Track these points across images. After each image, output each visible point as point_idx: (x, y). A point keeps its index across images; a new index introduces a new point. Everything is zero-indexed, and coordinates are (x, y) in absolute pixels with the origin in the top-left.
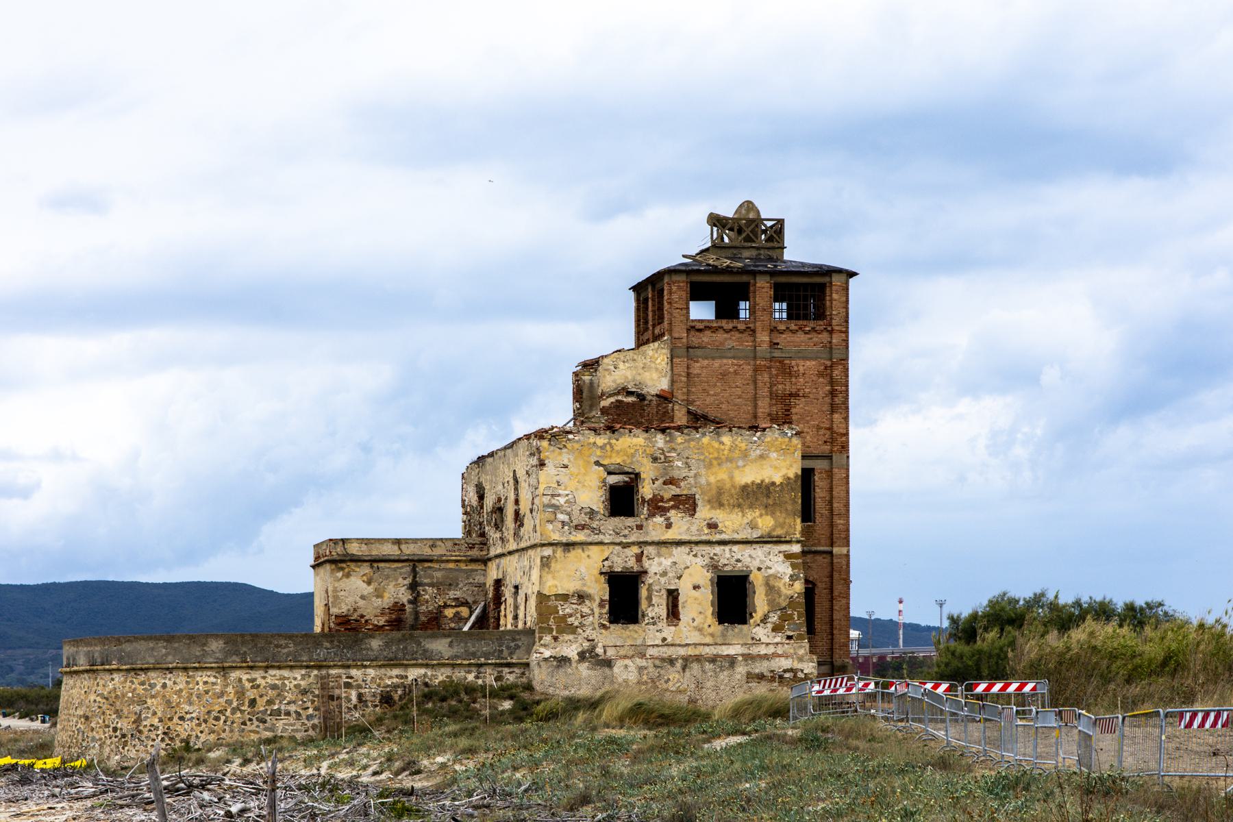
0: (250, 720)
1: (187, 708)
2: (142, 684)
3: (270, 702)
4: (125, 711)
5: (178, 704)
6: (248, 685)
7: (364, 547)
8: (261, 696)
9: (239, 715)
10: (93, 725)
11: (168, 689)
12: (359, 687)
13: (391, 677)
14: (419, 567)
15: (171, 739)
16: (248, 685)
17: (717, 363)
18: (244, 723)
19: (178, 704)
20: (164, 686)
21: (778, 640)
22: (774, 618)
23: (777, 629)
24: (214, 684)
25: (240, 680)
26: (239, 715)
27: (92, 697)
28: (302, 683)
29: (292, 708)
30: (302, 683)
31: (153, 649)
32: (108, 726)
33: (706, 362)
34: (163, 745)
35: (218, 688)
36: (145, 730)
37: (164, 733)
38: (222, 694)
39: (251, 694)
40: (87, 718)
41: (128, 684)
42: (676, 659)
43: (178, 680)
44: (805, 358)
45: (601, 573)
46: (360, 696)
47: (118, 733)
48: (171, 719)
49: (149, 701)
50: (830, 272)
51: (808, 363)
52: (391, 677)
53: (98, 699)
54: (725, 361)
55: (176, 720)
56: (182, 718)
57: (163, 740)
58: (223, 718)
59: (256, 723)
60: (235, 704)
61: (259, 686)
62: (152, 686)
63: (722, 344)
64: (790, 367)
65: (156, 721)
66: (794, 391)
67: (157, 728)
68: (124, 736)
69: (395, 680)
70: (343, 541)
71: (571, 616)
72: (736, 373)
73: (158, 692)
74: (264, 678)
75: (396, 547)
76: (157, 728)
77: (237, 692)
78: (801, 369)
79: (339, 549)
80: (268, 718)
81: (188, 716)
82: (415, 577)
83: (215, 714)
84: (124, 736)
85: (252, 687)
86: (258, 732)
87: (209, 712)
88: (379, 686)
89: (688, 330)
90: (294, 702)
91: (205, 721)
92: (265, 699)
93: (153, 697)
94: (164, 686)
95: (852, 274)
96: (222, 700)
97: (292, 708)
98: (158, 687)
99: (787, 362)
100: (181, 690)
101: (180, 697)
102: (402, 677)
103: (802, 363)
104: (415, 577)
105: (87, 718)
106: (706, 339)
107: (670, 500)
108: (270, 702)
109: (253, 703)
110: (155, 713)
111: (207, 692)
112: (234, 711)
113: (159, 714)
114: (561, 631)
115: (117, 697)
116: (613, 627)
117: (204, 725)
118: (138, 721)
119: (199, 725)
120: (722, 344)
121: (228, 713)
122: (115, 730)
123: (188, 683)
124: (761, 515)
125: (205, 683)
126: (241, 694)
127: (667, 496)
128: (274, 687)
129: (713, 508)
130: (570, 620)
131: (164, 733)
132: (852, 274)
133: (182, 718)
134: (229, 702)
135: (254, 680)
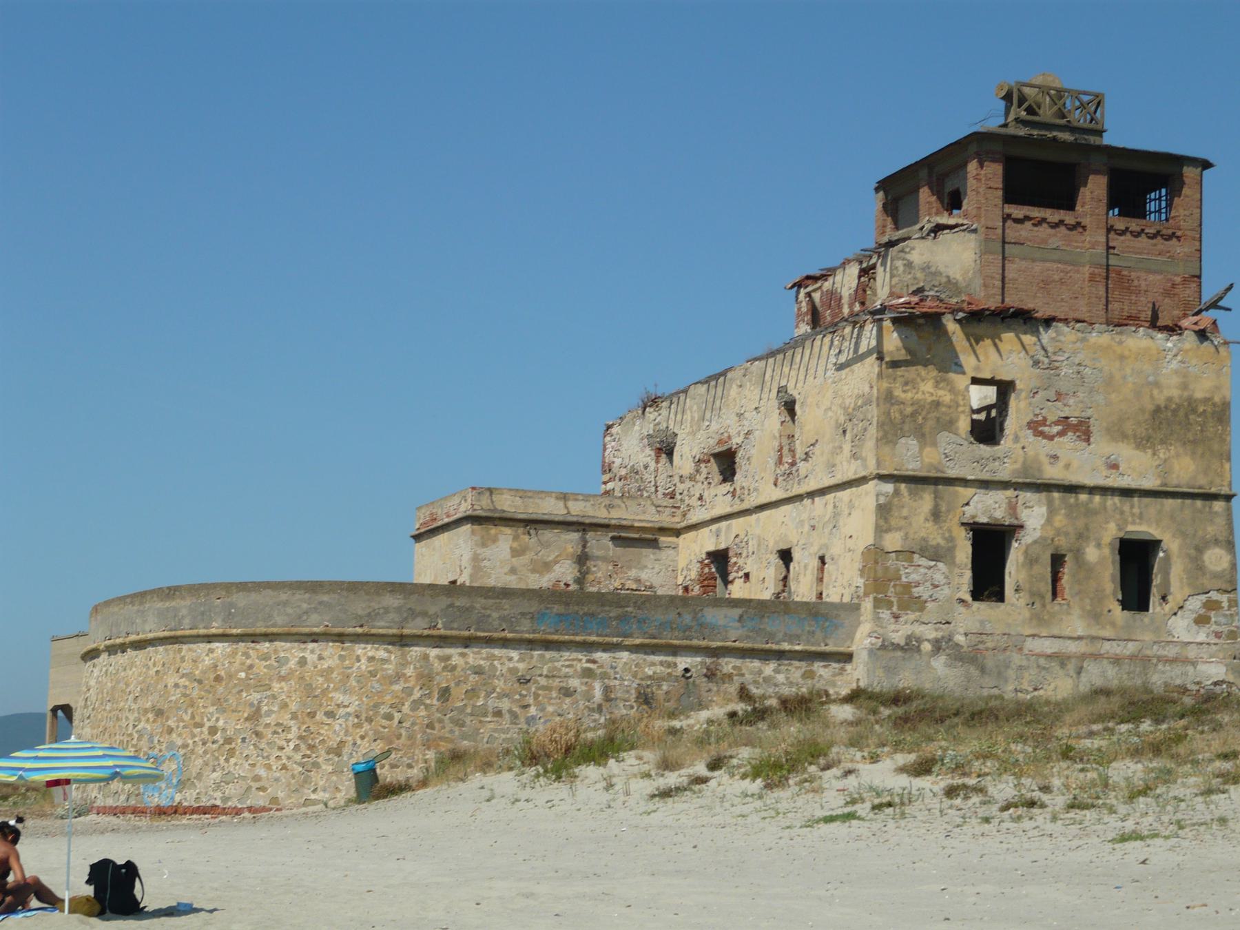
0: (440, 721)
1: (339, 697)
2: (265, 657)
3: (472, 693)
4: (232, 700)
5: (325, 692)
6: (438, 666)
7: (518, 501)
8: (458, 684)
9: (422, 712)
10: (171, 723)
11: (309, 667)
12: (604, 676)
13: (653, 664)
14: (590, 535)
15: (311, 747)
16: (438, 666)
17: (1038, 267)
18: (430, 726)
19: (325, 692)
20: (303, 662)
21: (1201, 637)
22: (1196, 604)
23: (1201, 621)
24: (384, 661)
25: (426, 657)
26: (422, 712)
27: (171, 680)
28: (521, 666)
29: (505, 705)
30: (521, 666)
31: (285, 604)
32: (201, 725)
33: (1024, 264)
34: (298, 757)
35: (390, 668)
36: (268, 733)
37: (301, 738)
38: (398, 676)
39: (443, 680)
40: (159, 713)
41: (239, 657)
42: (1069, 658)
43: (326, 654)
44: (1149, 271)
45: (963, 524)
46: (607, 690)
47: (218, 736)
48: (312, 715)
49: (276, 686)
50: (1180, 161)
51: (1151, 277)
52: (653, 664)
53: (183, 681)
54: (1048, 265)
55: (320, 716)
56: (330, 714)
57: (297, 748)
58: (397, 716)
59: (449, 726)
60: (417, 694)
61: (454, 668)
62: (281, 662)
63: (1044, 241)
64: (1130, 280)
65: (286, 718)
66: (1134, 312)
67: (286, 729)
68: (228, 741)
69: (659, 669)
70: (491, 491)
71: (918, 584)
72: (1062, 282)
73: (292, 672)
74: (463, 655)
75: (561, 504)
76: (286, 729)
77: (420, 676)
78: (1143, 284)
79: (485, 502)
80: (468, 720)
81: (342, 711)
82: (584, 546)
83: (384, 710)
84: (228, 741)
85: (445, 668)
86: (451, 741)
87: (376, 706)
88: (635, 676)
89: (1004, 221)
90: (506, 695)
91: (369, 720)
92: (465, 687)
93: (282, 679)
94: (303, 662)
95: (1206, 165)
96: (397, 687)
97: (505, 705)
98: (292, 664)
99: (1125, 273)
100: (330, 670)
101: (328, 680)
102: (669, 665)
103: (1143, 275)
104: (584, 546)
105: (159, 713)
106: (1024, 233)
107: (1056, 423)
108: (472, 693)
109: (445, 693)
110: (284, 706)
111: (373, 674)
112: (416, 705)
113: (293, 707)
114: (904, 606)
115: (218, 679)
116: (976, 604)
117: (366, 726)
118: (255, 716)
119: (359, 725)
120: (1044, 241)
121: (406, 708)
122: (213, 730)
123: (342, 658)
124: (1178, 455)
125: (371, 659)
126: (426, 678)
127: (1051, 418)
128: (478, 671)
129: (1114, 439)
130: (916, 591)
131: (301, 738)
132: (1206, 165)
133: (330, 714)
134: (408, 691)
135: (448, 658)
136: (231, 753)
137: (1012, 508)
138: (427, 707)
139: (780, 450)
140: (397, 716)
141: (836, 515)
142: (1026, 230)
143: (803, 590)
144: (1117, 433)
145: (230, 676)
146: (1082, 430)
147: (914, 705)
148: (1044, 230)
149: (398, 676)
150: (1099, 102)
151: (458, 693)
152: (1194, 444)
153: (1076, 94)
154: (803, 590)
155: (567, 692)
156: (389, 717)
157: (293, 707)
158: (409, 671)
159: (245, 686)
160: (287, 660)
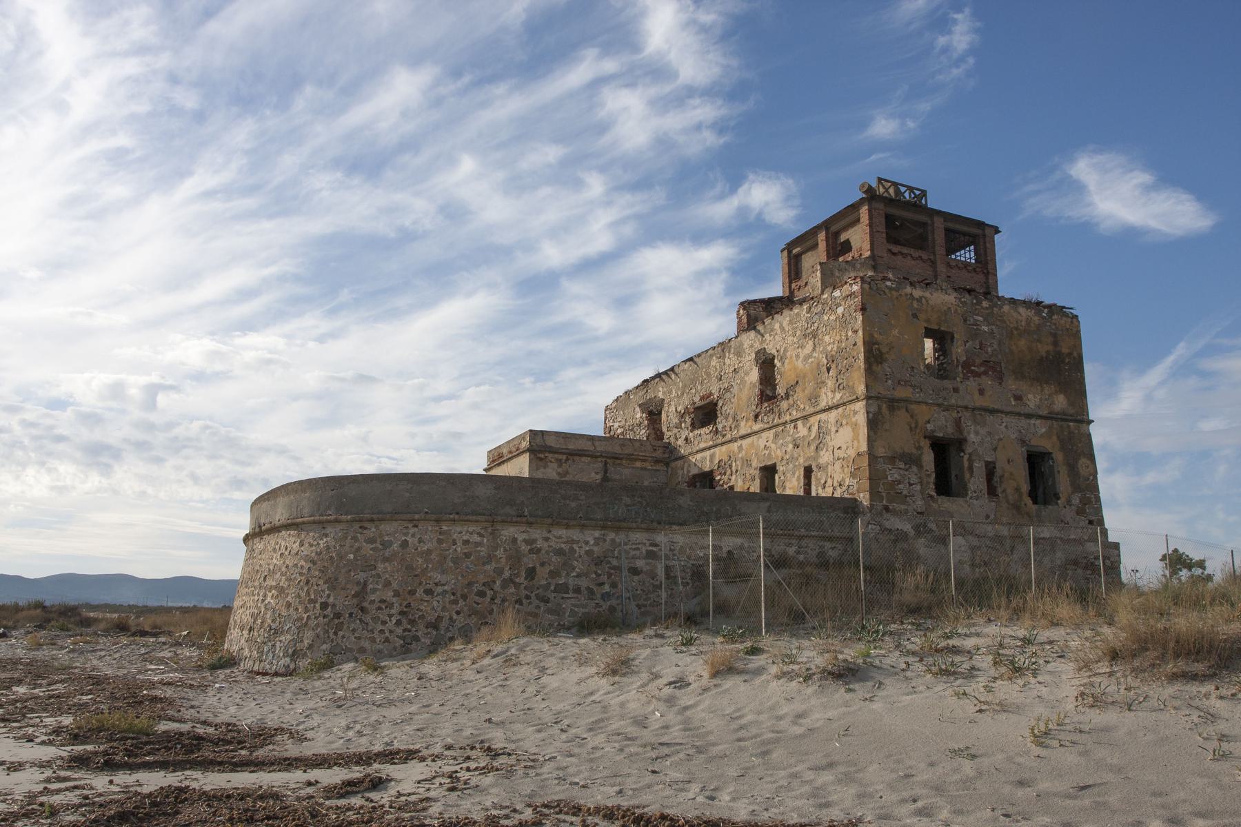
1: (438, 577)
5: (424, 571)
16: (524, 548)
19: (424, 571)
29: (584, 583)
35: (483, 551)
38: (490, 558)
58: (489, 593)
59: (536, 602)
67: (391, 606)
68: (338, 615)
76: (391, 606)
77: (509, 558)
87: (470, 584)
91: (464, 597)
93: (386, 560)
100: (429, 552)
110: (388, 584)
113: (395, 585)
117: (461, 603)
118: (361, 593)
136: (339, 627)
137: (958, 422)
138: (517, 585)
140: (489, 593)
142: (899, 260)
149: (490, 558)
150: (924, 193)
151: (542, 572)
156: (482, 594)
157: (395, 585)
158: (500, 553)
160: (391, 543)
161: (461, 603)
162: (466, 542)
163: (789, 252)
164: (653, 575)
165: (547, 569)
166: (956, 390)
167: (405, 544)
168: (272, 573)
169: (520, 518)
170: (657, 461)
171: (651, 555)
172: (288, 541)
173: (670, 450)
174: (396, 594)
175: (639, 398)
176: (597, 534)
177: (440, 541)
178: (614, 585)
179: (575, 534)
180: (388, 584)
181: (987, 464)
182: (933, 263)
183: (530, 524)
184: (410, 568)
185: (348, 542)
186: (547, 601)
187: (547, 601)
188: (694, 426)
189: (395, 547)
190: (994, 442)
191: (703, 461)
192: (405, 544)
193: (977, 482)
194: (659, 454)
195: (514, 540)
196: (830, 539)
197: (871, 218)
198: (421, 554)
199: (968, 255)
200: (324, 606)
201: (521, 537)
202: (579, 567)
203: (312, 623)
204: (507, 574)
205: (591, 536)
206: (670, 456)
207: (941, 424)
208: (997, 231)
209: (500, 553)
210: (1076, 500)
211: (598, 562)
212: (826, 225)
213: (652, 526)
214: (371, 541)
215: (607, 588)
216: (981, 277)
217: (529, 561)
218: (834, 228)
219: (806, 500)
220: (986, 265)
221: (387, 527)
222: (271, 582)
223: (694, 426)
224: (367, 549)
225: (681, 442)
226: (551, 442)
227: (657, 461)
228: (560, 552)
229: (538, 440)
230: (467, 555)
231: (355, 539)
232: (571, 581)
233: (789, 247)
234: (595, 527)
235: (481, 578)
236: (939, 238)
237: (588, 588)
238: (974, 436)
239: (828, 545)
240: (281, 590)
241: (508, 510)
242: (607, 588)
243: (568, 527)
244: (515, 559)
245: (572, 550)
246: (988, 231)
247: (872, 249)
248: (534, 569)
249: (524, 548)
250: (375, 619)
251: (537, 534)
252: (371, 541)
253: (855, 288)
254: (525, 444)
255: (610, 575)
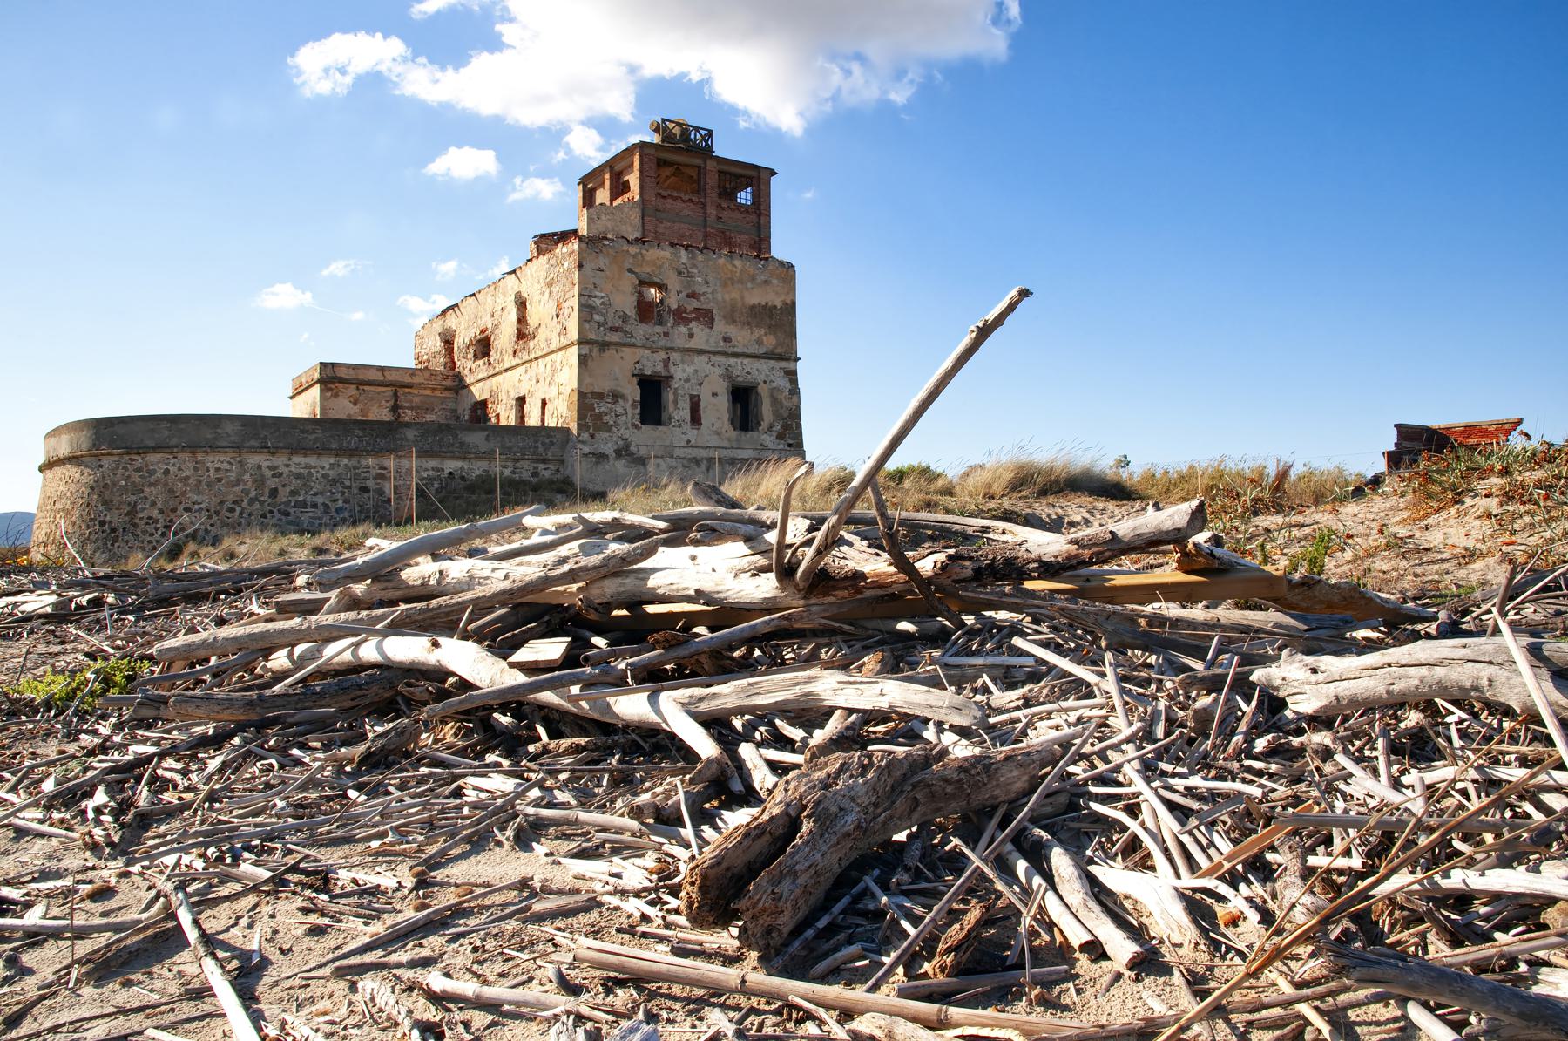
1: (195, 498)
5: (184, 493)
16: (268, 473)
19: (184, 493)
29: (320, 500)
35: (233, 476)
38: (238, 482)
49: (147, 490)
58: (238, 509)
59: (278, 515)
65: (155, 513)
67: (157, 521)
68: (114, 530)
76: (157, 521)
77: (255, 481)
83: (228, 504)
87: (222, 503)
91: (217, 513)
93: (151, 485)
100: (187, 478)
102: (438, 470)
110: (153, 504)
113: (159, 505)
114: (597, 429)
117: (215, 518)
118: (132, 512)
121: (245, 504)
127: (690, 308)
136: (115, 540)
137: (666, 362)
138: (262, 503)
139: (1117, 491)
140: (238, 509)
141: (553, 372)
142: (669, 203)
143: (533, 420)
144: (731, 318)
145: (114, 484)
146: (706, 317)
147: (464, 547)
148: (679, 204)
149: (238, 482)
150: (710, 134)
151: (283, 496)
152: (772, 329)
153: (697, 129)
154: (533, 420)
155: (365, 490)
156: (232, 510)
157: (159, 505)
158: (247, 477)
159: (124, 490)
160: (155, 471)
161: (215, 518)
162: (218, 469)
163: (585, 186)
164: (381, 492)
165: (288, 489)
166: (666, 334)
167: (167, 472)
168: (60, 498)
169: (263, 448)
170: (447, 389)
171: (381, 477)
172: (71, 471)
173: (459, 378)
174: (162, 511)
175: (438, 326)
176: (332, 460)
177: (196, 469)
178: (346, 501)
179: (312, 460)
180: (153, 504)
181: (692, 397)
182: (704, 205)
183: (273, 454)
184: (171, 491)
185: (120, 471)
186: (287, 514)
187: (287, 514)
188: (476, 357)
189: (159, 475)
190: (700, 377)
191: (479, 392)
192: (167, 472)
193: (682, 413)
194: (449, 383)
195: (260, 467)
196: (544, 461)
197: (641, 163)
198: (181, 479)
199: (745, 197)
200: (102, 523)
201: (265, 464)
202: (316, 487)
203: (93, 537)
204: (253, 494)
205: (327, 461)
206: (458, 385)
207: (652, 364)
208: (773, 173)
209: (247, 477)
210: (778, 427)
211: (334, 482)
212: (609, 165)
213: (379, 452)
214: (139, 470)
215: (340, 503)
216: (754, 218)
217: (272, 483)
218: (617, 168)
219: (520, 429)
220: (761, 207)
221: (153, 458)
222: (59, 506)
223: (476, 357)
224: (136, 477)
225: (466, 372)
226: (342, 373)
227: (447, 389)
228: (299, 476)
229: (329, 372)
230: (219, 480)
231: (125, 469)
232: (309, 499)
233: (584, 181)
234: (330, 455)
235: (231, 498)
236: (712, 180)
237: (324, 504)
238: (681, 372)
239: (541, 466)
240: (67, 512)
241: (253, 442)
242: (340, 503)
243: (305, 455)
244: (260, 482)
245: (310, 474)
246: (763, 175)
247: (641, 194)
248: (276, 490)
249: (268, 473)
250: (144, 532)
251: (280, 460)
252: (139, 470)
253: (576, 247)
254: (317, 376)
255: (343, 493)
